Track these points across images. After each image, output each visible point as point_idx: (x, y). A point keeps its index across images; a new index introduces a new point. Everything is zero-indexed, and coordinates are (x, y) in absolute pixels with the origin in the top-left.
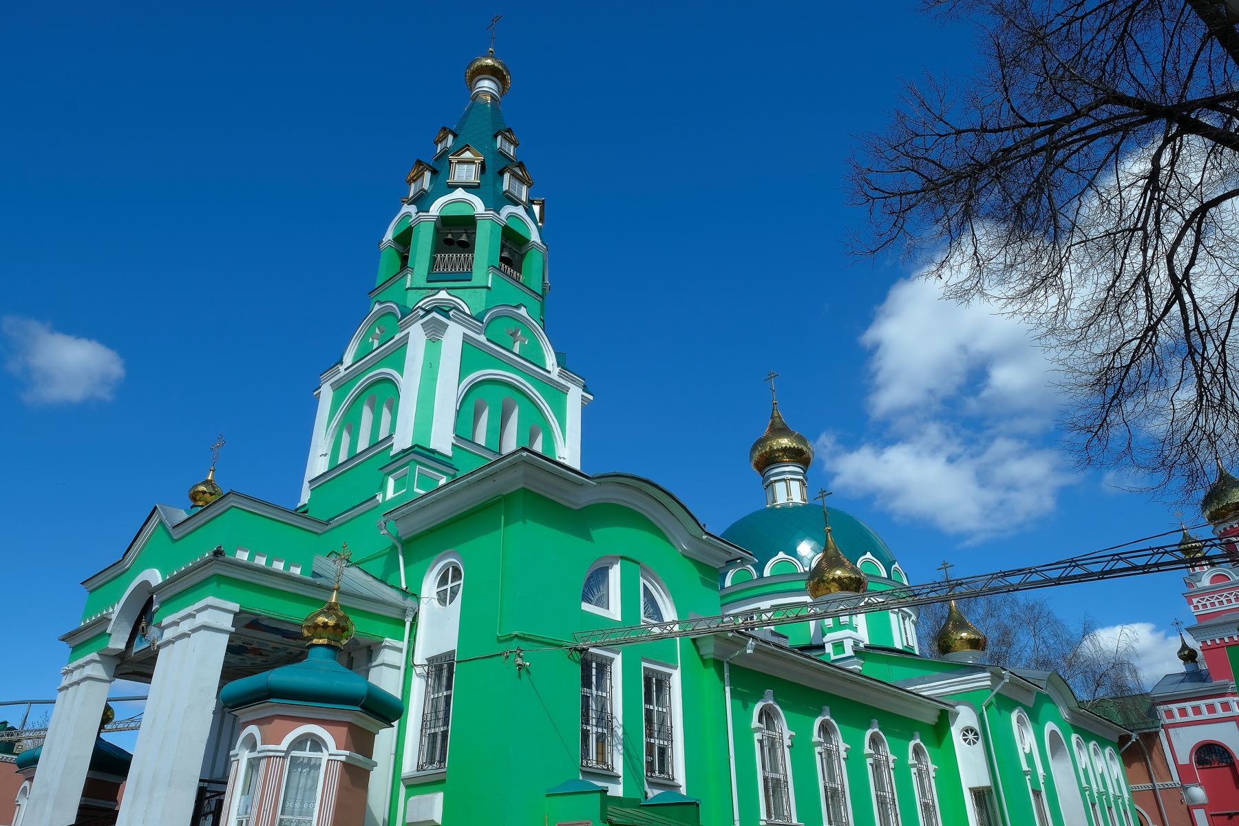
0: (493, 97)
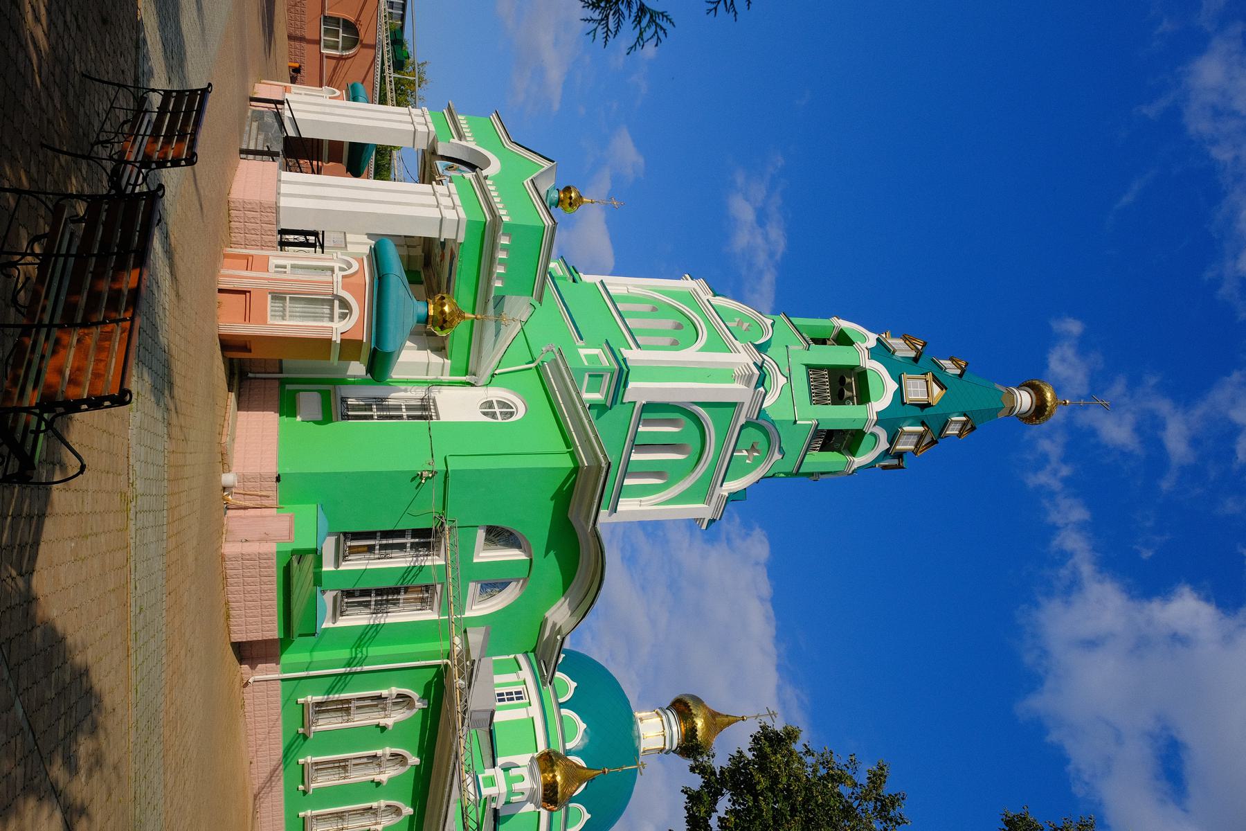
0: (1013, 409)
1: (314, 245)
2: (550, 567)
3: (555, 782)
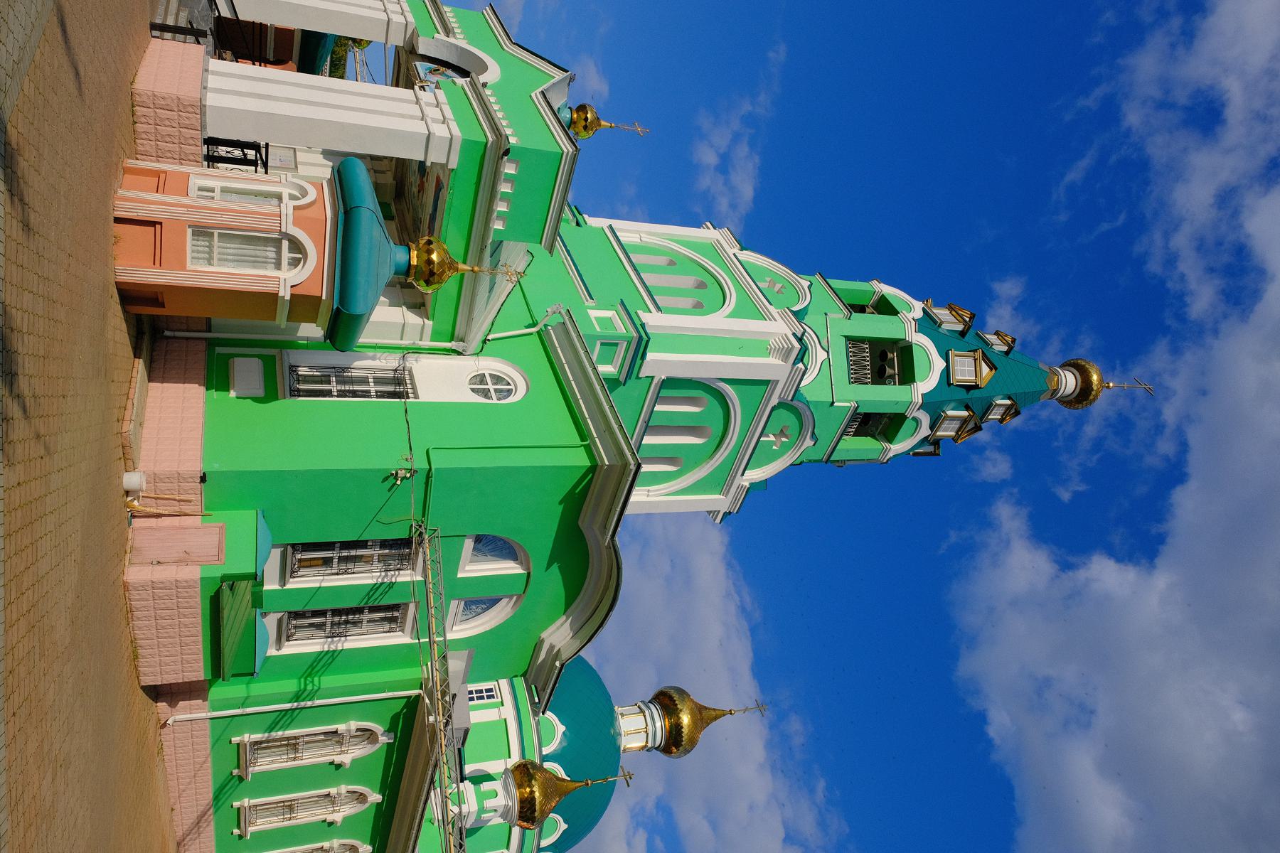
0: (1055, 391)
1: (253, 163)
2: (552, 583)
3: (534, 799)
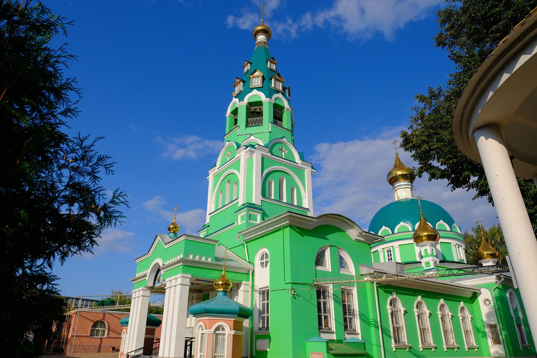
0: (265, 43)
1: (191, 342)
2: (333, 238)
